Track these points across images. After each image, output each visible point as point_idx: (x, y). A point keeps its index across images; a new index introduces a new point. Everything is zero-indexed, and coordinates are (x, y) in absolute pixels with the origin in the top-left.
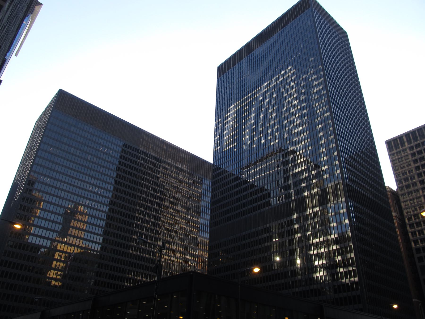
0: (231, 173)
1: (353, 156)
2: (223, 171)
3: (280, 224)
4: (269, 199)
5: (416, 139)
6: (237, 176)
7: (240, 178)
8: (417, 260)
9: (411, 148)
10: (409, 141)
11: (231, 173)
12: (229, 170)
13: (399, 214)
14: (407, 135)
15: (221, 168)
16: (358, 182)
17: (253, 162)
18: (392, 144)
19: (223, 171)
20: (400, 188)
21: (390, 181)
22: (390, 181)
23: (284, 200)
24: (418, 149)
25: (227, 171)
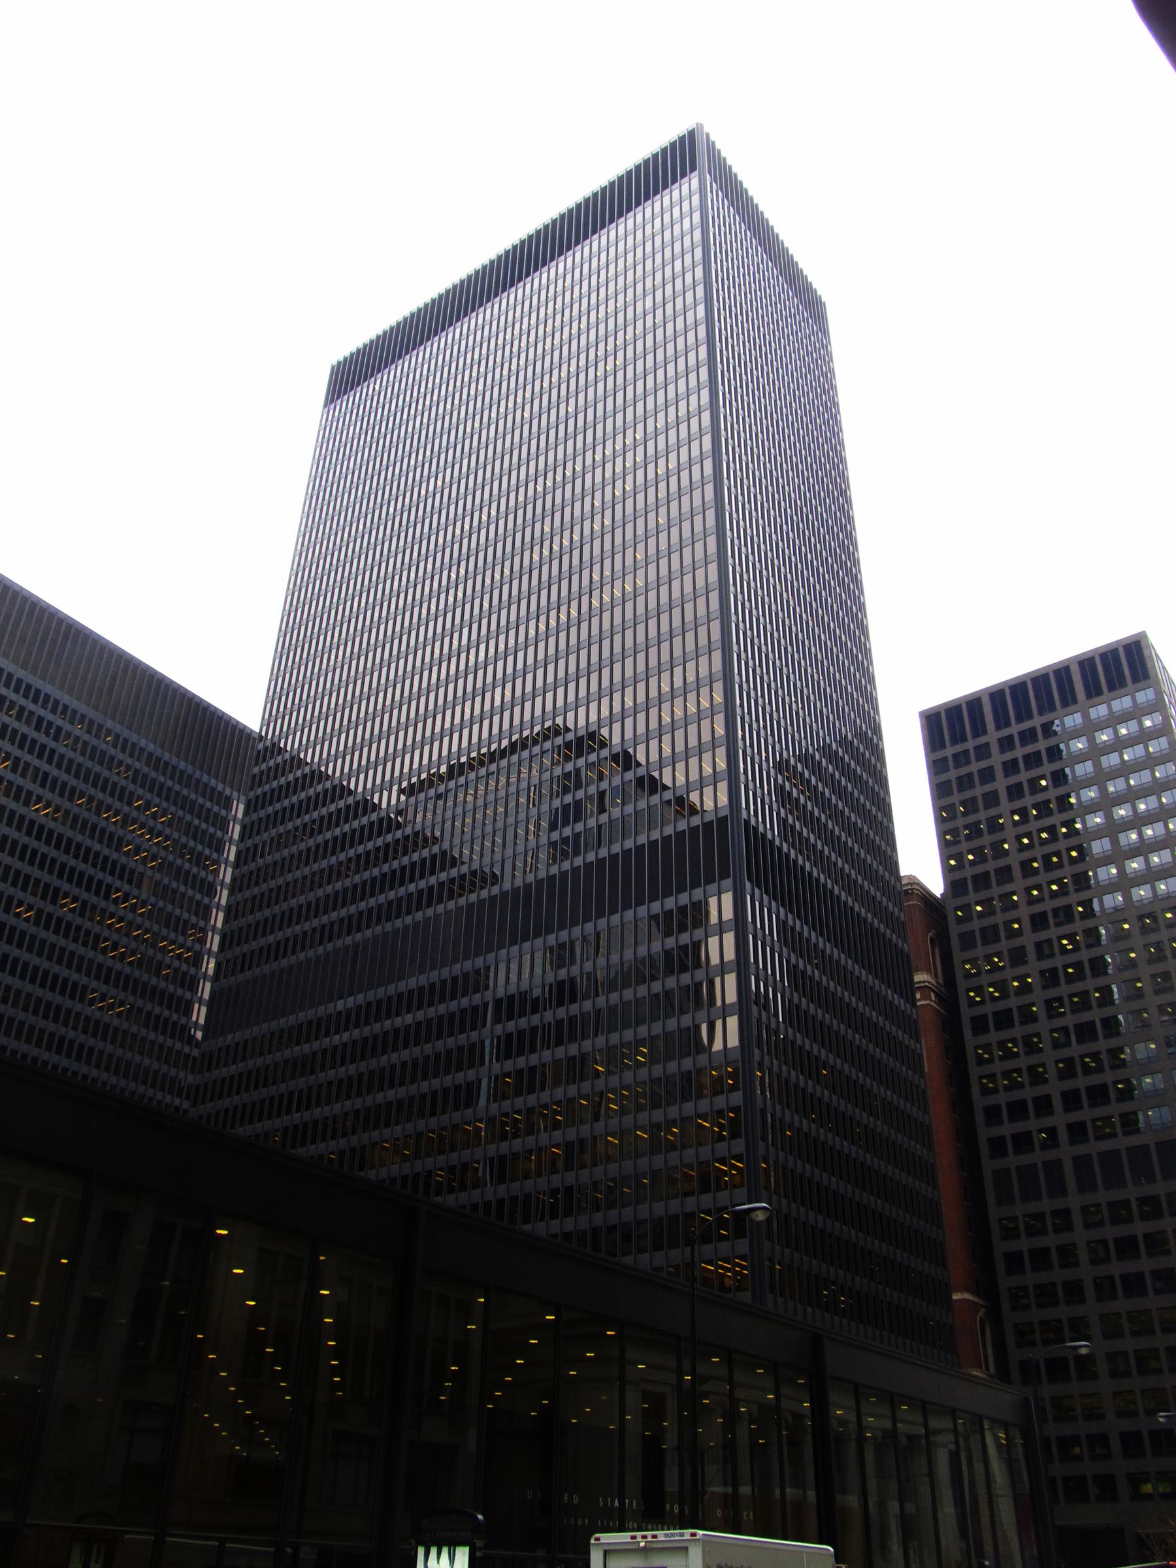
0: (293, 758)
1: (813, 757)
2: (357, 803)
3: (492, 1159)
4: (699, 933)
5: (1023, 713)
6: (337, 782)
7: (301, 763)
8: (984, 1149)
9: (1006, 744)
10: (1002, 721)
11: (293, 758)
12: (358, 785)
13: (941, 981)
14: (997, 695)
15: (350, 792)
16: (846, 843)
17: (443, 769)
18: (947, 727)
19: (357, 803)
20: (955, 885)
21: (920, 857)
22: (920, 857)
23: (713, 901)
24: (1030, 749)
25: (376, 808)
